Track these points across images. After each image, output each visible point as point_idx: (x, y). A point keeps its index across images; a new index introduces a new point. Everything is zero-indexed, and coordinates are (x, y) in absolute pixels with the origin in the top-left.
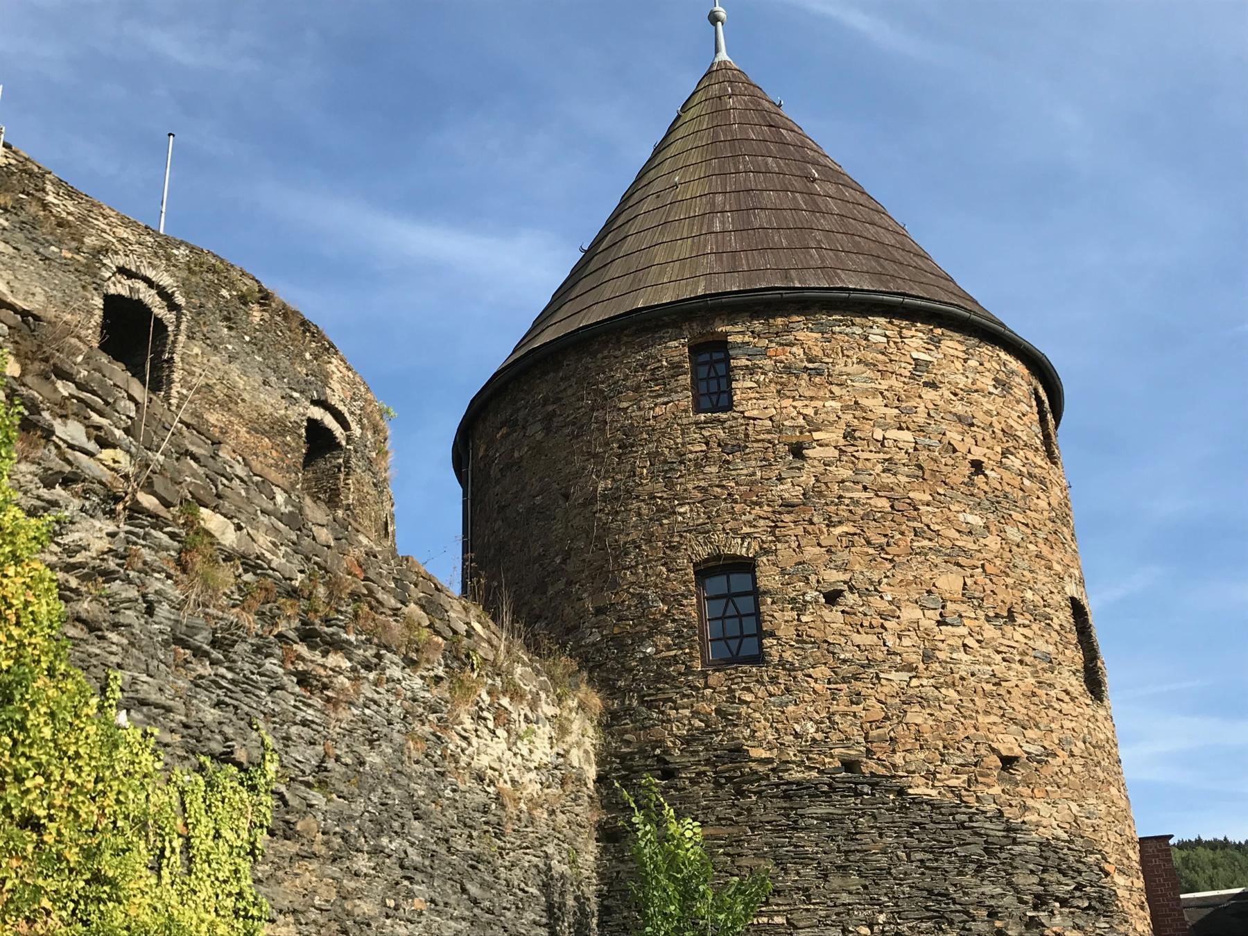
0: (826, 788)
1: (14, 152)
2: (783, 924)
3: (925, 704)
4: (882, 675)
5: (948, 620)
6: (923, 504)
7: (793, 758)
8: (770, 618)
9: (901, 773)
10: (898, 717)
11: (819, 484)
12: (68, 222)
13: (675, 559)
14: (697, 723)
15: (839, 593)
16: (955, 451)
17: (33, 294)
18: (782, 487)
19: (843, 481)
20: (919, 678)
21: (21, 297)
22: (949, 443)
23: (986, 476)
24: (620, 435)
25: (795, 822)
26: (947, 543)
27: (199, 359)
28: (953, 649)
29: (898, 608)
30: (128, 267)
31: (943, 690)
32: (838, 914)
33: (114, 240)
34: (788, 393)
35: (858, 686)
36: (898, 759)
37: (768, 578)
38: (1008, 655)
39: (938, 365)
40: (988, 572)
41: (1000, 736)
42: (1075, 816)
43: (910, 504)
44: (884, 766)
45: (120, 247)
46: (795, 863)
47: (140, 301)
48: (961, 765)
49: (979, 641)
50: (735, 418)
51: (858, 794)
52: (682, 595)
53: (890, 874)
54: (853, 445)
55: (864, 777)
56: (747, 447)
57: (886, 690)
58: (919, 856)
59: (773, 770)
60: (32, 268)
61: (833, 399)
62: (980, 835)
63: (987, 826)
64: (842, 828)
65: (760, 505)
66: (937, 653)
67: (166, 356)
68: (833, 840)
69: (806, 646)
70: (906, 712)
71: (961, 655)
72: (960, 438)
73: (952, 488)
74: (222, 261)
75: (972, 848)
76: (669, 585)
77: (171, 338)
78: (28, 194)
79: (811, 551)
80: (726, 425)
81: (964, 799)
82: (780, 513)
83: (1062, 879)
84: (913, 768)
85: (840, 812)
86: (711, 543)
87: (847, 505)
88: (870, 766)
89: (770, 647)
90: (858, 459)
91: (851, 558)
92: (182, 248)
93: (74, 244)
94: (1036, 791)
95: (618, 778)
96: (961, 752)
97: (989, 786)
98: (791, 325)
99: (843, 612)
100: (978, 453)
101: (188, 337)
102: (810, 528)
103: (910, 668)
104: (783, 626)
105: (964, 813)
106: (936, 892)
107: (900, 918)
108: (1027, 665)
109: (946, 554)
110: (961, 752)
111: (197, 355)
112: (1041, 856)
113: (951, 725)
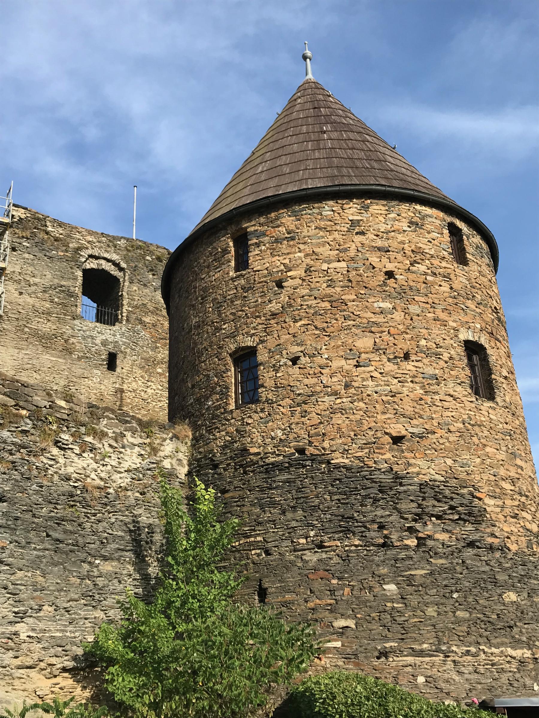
0: (287, 465)
1: (29, 211)
2: (261, 541)
3: (344, 412)
4: (319, 400)
5: (361, 364)
6: (350, 301)
7: (270, 451)
8: (262, 377)
9: (327, 452)
10: (327, 421)
11: (290, 301)
12: (60, 238)
13: (221, 354)
14: (228, 438)
15: (298, 358)
16: (374, 268)
17: (45, 275)
18: (270, 305)
19: (303, 297)
20: (341, 398)
21: (39, 277)
22: (370, 264)
23: (396, 279)
24: (202, 293)
25: (271, 485)
26: (365, 321)
27: (137, 292)
28: (364, 380)
29: (331, 361)
30: (94, 254)
31: (355, 404)
32: (289, 533)
33: (86, 243)
34: (276, 254)
35: (305, 407)
36: (326, 444)
37: (262, 356)
38: (402, 379)
39: (367, 221)
40: (392, 333)
41: (392, 426)
42: (450, 467)
43: (342, 303)
44: (318, 449)
45: (89, 245)
46: (269, 507)
47: (103, 269)
48: (364, 444)
49: (381, 373)
50: (249, 273)
51: (304, 466)
52: (223, 372)
53: (319, 508)
54: (310, 276)
55: (307, 457)
56: (254, 287)
57: (321, 407)
58: (336, 497)
59: (261, 458)
60: (43, 263)
61: (300, 252)
62: (376, 482)
63: (381, 477)
64: (294, 486)
65: (259, 317)
66: (353, 383)
67: (120, 294)
68: (290, 493)
69: (279, 389)
70: (332, 418)
71: (370, 383)
72: (379, 260)
73: (371, 289)
74: (145, 243)
75: (372, 490)
76: (219, 368)
77: (122, 284)
78: (38, 229)
79: (285, 337)
80: (245, 277)
81: (366, 463)
82: (269, 320)
83: (436, 503)
84: (334, 448)
85: (294, 477)
86: (236, 342)
87: (305, 309)
88: (310, 450)
89: (262, 393)
90: (312, 282)
91: (305, 338)
92: (122, 240)
93: (64, 248)
94: (416, 454)
95: (195, 472)
96: (365, 437)
97: (382, 454)
98: (279, 216)
99: (300, 368)
100: (390, 267)
101: (130, 283)
102: (284, 325)
103: (335, 393)
104: (268, 380)
105: (367, 471)
106: (346, 516)
107: (323, 533)
108: (416, 383)
109: (363, 327)
110: (365, 437)
111: (135, 290)
112: (420, 492)
113: (360, 422)
